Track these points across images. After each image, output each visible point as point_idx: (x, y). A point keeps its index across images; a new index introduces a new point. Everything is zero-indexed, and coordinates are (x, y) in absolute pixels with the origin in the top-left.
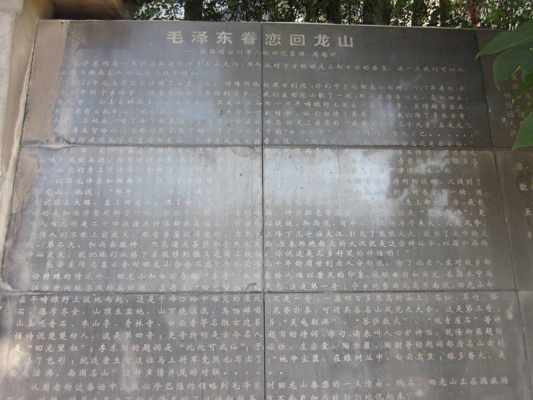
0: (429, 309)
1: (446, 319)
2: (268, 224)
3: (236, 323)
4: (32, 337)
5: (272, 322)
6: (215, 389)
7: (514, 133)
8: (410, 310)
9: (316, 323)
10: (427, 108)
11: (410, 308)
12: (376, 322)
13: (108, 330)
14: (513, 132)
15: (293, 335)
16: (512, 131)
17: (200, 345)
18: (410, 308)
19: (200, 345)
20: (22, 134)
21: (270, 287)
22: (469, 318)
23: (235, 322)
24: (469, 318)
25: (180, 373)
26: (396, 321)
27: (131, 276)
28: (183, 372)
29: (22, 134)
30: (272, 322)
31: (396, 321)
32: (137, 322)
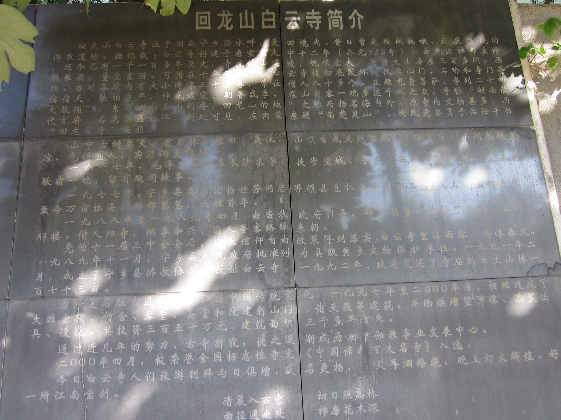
0: (203, 358)
1: (410, 80)
2: (379, 268)
3: (190, 345)
4: (263, 298)
5: (288, 371)
6: (356, 242)
7: (52, 120)
8: (277, 341)
9: (483, 92)
10: (330, 243)
11: (277, 338)
12: (434, 81)
13: (139, 266)
14: (51, 119)
15: (264, 106)
16: (50, 118)
17: (201, 115)
18: (277, 338)
19: (201, 115)
20: (419, 282)
21: (74, 157)
22: (446, 68)
23: (189, 344)
24: (446, 68)
25: (178, 143)
26: (502, 358)
27: (76, 131)
28: (181, 142)
29: (419, 282)
30: (288, 371)
31: (502, 358)
32: (96, 207)
